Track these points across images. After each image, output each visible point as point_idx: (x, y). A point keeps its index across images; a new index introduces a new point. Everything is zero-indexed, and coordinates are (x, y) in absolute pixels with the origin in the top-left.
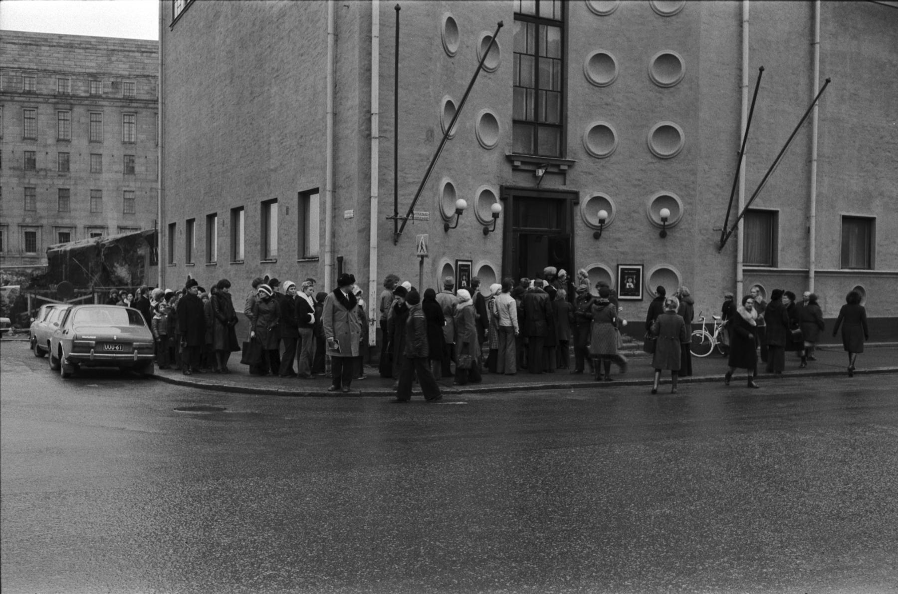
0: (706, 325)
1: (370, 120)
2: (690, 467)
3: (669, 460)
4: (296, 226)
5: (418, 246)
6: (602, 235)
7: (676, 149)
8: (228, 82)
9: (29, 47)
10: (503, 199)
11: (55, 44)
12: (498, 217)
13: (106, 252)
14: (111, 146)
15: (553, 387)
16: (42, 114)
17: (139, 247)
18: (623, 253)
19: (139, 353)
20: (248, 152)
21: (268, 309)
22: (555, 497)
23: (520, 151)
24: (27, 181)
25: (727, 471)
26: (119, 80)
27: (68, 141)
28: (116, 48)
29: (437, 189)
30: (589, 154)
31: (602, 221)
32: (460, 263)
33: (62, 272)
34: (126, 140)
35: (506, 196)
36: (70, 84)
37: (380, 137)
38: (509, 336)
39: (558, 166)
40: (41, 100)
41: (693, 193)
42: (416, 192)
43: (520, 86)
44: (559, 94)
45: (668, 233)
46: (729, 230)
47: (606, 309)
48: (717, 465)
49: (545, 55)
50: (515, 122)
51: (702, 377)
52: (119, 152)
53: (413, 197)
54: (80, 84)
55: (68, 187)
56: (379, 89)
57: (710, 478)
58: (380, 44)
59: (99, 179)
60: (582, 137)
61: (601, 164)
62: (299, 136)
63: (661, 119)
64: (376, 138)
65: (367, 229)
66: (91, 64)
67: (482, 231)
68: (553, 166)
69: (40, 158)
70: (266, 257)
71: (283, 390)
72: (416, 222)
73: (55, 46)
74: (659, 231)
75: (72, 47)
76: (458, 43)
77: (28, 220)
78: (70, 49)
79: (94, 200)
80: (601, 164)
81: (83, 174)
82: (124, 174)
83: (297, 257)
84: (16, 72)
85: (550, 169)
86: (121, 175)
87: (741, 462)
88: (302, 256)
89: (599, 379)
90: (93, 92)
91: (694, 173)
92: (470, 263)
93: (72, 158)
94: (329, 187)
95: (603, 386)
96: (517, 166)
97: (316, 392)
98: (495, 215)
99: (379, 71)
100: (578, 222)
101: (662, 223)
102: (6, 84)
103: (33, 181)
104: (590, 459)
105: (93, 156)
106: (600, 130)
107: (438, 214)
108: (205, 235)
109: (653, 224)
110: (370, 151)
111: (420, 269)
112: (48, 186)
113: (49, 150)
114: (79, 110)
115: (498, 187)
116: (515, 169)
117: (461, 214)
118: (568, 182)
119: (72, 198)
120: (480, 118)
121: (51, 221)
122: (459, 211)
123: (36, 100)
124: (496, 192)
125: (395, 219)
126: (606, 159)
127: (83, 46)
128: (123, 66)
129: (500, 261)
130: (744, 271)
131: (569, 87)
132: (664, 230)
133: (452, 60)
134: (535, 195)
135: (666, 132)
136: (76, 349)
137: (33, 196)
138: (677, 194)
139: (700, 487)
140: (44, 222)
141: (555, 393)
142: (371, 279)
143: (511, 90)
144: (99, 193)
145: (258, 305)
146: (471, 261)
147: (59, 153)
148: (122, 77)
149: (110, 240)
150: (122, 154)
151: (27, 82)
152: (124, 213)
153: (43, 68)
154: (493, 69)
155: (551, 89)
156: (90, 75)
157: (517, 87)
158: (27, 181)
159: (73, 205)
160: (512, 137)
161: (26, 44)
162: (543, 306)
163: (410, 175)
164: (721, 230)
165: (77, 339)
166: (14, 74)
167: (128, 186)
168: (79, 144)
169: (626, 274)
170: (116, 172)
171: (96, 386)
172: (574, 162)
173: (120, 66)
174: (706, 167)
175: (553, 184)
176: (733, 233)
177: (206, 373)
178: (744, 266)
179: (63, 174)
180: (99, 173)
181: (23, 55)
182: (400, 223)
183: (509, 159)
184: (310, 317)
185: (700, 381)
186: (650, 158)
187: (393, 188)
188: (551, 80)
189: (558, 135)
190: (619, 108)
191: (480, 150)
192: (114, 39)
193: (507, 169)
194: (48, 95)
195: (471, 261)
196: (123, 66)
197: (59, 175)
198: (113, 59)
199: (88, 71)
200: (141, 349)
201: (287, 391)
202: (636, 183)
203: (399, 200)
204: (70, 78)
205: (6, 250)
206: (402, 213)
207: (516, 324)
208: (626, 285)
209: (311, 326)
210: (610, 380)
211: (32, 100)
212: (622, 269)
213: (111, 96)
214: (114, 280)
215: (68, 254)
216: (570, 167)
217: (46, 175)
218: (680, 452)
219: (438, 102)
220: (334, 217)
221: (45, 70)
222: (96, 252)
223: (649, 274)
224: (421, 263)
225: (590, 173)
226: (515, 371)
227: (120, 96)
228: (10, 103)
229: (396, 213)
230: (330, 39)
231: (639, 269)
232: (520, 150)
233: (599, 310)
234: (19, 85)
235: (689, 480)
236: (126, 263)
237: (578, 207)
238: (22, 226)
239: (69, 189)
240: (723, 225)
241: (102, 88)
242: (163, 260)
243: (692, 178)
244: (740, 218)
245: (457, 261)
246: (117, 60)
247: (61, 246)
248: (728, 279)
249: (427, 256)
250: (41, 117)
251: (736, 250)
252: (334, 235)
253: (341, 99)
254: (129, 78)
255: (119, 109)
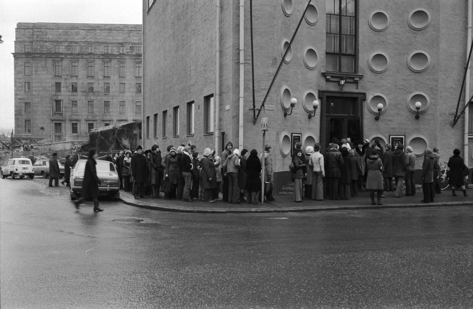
0: (447, 171)
1: (239, 54)
2: (417, 273)
3: (404, 266)
4: (203, 115)
5: (262, 125)
6: (380, 118)
7: (425, 67)
8: (172, 39)
9: (90, 31)
10: (320, 98)
11: (103, 29)
12: (317, 108)
13: (118, 132)
14: (130, 80)
15: (345, 208)
16: (96, 64)
17: (134, 130)
18: (392, 128)
19: (110, 187)
20: (181, 76)
21: (175, 161)
22: (311, 296)
23: (331, 70)
24: (89, 98)
25: (445, 277)
26: (134, 45)
27: (109, 77)
28: (132, 29)
29: (280, 92)
30: (372, 71)
31: (380, 110)
32: (293, 135)
33: (96, 143)
34: (137, 76)
35: (321, 96)
36: (110, 49)
37: (245, 63)
38: (319, 177)
39: (353, 78)
40: (96, 57)
41: (435, 92)
42: (266, 94)
43: (330, 33)
44: (354, 37)
45: (420, 116)
46: (459, 114)
47: (376, 162)
48: (438, 272)
49: (345, 15)
50: (327, 53)
51: (440, 204)
52: (134, 82)
53: (264, 97)
54: (115, 48)
55: (109, 100)
56: (244, 36)
57: (431, 283)
58: (244, 10)
59: (124, 96)
60: (368, 62)
61: (380, 76)
62: (204, 65)
63: (416, 49)
64: (242, 64)
65: (237, 116)
66: (120, 38)
67: (307, 117)
68: (350, 78)
69: (95, 86)
70: (189, 133)
71: (182, 209)
72: (266, 111)
73: (103, 30)
74: (415, 115)
75: (111, 30)
76: (292, 9)
77: (90, 117)
78: (110, 31)
79: (121, 106)
80: (380, 76)
81: (116, 94)
82: (136, 93)
83: (203, 133)
84: (84, 44)
85: (348, 80)
86: (134, 94)
87: (456, 269)
88: (206, 132)
89: (374, 204)
90: (121, 52)
91: (436, 80)
92: (300, 135)
93: (111, 86)
94: (218, 92)
95: (376, 208)
96: (329, 79)
97: (200, 210)
98: (315, 107)
99: (244, 26)
100: (366, 111)
101: (416, 111)
102: (79, 50)
103: (92, 98)
104: (349, 263)
105: (121, 84)
106: (379, 57)
107: (280, 107)
108: (162, 122)
109: (411, 111)
110: (239, 71)
111: (263, 138)
112: (99, 100)
113: (100, 82)
114: (114, 62)
115: (317, 91)
116: (327, 80)
117: (294, 106)
118: (359, 87)
119: (111, 106)
120: (306, 51)
121: (101, 118)
122: (293, 105)
123: (94, 57)
124: (316, 94)
125: (254, 110)
126: (383, 74)
127: (116, 29)
128: (136, 38)
129: (318, 135)
130: (469, 138)
131: (360, 32)
132: (417, 115)
133: (289, 18)
134: (339, 95)
135: (419, 57)
136: (77, 184)
137: (92, 105)
138: (426, 93)
139: (421, 291)
140: (97, 118)
141: (344, 212)
142: (240, 144)
143: (325, 35)
144: (123, 103)
145: (169, 159)
146: (301, 134)
147: (105, 83)
148: (135, 44)
149: (120, 126)
150: (135, 83)
151: (89, 48)
152: (136, 113)
153: (97, 41)
154: (314, 23)
155: (349, 34)
156: (120, 43)
157: (328, 34)
158: (89, 98)
159: (111, 110)
160: (325, 62)
161: (89, 30)
162: (338, 159)
163: (262, 85)
164: (453, 114)
165: (77, 179)
166: (83, 45)
167: (138, 99)
168: (114, 79)
169: (394, 141)
170: (132, 92)
171: (84, 205)
172: (363, 76)
173: (134, 38)
174: (444, 76)
175: (350, 88)
176: (462, 116)
177: (147, 198)
178: (469, 136)
179: (106, 93)
180: (124, 93)
181: (88, 35)
182: (257, 113)
183: (324, 75)
184: (191, 165)
185: (439, 206)
186: (408, 72)
187: (252, 92)
188: (349, 29)
189: (354, 60)
190: (390, 43)
191: (306, 70)
192: (131, 25)
193: (323, 81)
194: (100, 54)
195: (301, 134)
196: (136, 38)
197: (105, 95)
198: (131, 35)
199: (119, 41)
200: (111, 184)
201: (184, 209)
202: (401, 87)
203: (256, 99)
204: (110, 45)
205: (79, 132)
206: (258, 106)
207: (323, 169)
208: (394, 147)
209: (191, 171)
210: (381, 205)
211: (92, 57)
212: (392, 138)
213: (130, 54)
214: (122, 147)
215: (99, 134)
216: (360, 78)
217: (98, 94)
218: (413, 259)
219: (280, 42)
220: (220, 110)
221: (98, 42)
222: (113, 133)
223: (409, 140)
224: (264, 134)
225: (373, 82)
226: (322, 198)
227: (134, 53)
228: (81, 59)
229: (254, 106)
230: (218, 9)
231: (403, 138)
232: (330, 70)
233: (372, 163)
234: (86, 50)
235: (414, 284)
236: (128, 138)
237: (366, 102)
238: (87, 120)
239: (109, 102)
240: (455, 111)
241: (125, 50)
242: (144, 136)
243: (435, 83)
244: (465, 107)
245: (292, 134)
246: (133, 36)
247: (96, 129)
248: (459, 143)
249: (267, 130)
250: (97, 66)
251: (464, 126)
252: (220, 120)
253: (224, 43)
254: (138, 44)
255: (133, 60)
